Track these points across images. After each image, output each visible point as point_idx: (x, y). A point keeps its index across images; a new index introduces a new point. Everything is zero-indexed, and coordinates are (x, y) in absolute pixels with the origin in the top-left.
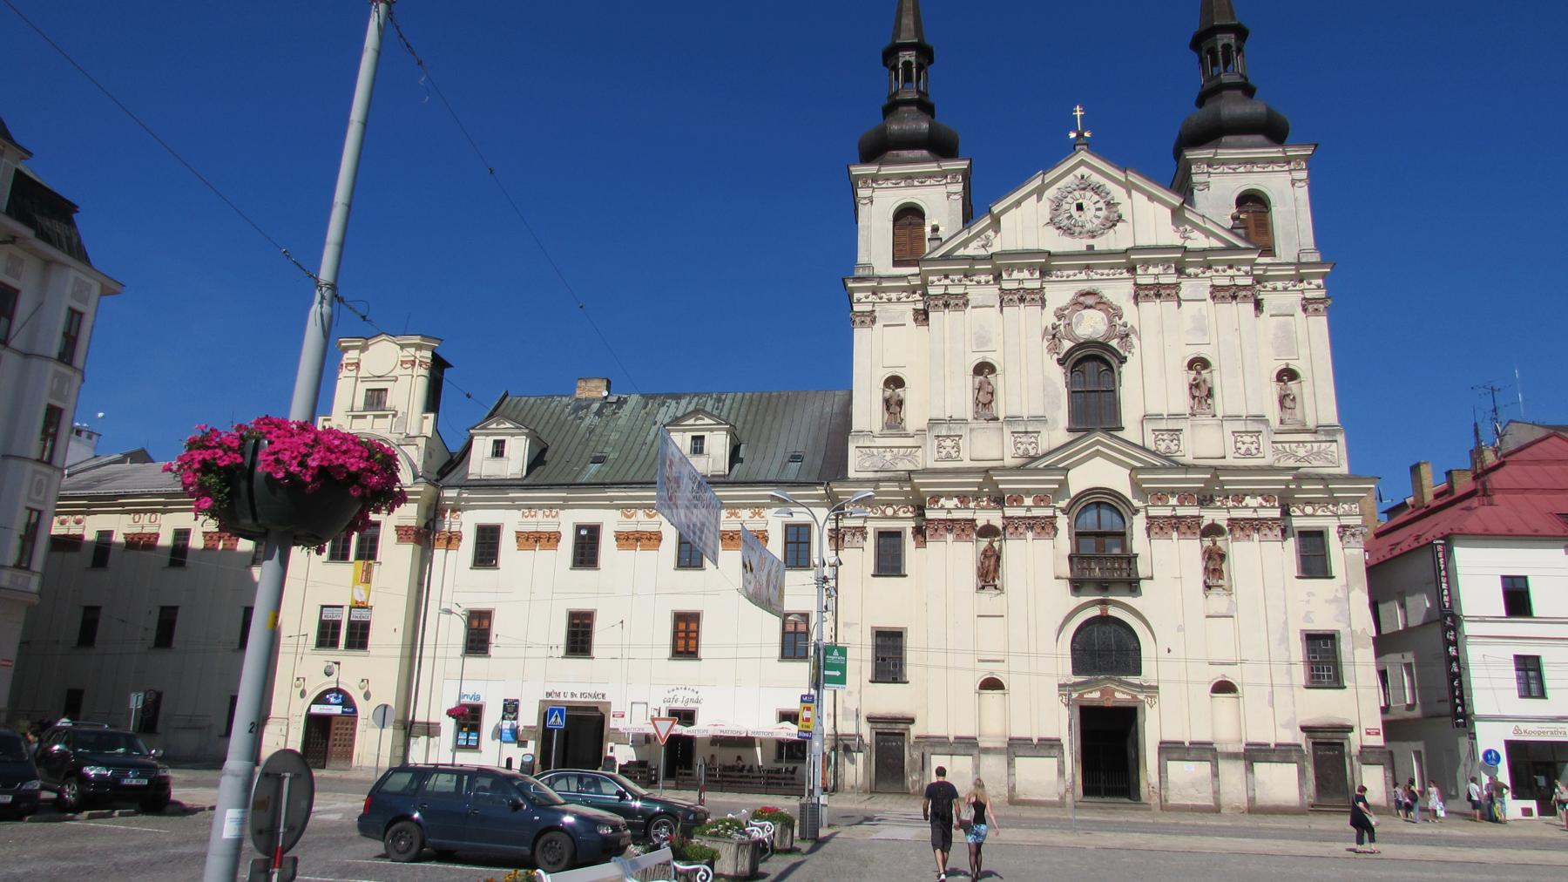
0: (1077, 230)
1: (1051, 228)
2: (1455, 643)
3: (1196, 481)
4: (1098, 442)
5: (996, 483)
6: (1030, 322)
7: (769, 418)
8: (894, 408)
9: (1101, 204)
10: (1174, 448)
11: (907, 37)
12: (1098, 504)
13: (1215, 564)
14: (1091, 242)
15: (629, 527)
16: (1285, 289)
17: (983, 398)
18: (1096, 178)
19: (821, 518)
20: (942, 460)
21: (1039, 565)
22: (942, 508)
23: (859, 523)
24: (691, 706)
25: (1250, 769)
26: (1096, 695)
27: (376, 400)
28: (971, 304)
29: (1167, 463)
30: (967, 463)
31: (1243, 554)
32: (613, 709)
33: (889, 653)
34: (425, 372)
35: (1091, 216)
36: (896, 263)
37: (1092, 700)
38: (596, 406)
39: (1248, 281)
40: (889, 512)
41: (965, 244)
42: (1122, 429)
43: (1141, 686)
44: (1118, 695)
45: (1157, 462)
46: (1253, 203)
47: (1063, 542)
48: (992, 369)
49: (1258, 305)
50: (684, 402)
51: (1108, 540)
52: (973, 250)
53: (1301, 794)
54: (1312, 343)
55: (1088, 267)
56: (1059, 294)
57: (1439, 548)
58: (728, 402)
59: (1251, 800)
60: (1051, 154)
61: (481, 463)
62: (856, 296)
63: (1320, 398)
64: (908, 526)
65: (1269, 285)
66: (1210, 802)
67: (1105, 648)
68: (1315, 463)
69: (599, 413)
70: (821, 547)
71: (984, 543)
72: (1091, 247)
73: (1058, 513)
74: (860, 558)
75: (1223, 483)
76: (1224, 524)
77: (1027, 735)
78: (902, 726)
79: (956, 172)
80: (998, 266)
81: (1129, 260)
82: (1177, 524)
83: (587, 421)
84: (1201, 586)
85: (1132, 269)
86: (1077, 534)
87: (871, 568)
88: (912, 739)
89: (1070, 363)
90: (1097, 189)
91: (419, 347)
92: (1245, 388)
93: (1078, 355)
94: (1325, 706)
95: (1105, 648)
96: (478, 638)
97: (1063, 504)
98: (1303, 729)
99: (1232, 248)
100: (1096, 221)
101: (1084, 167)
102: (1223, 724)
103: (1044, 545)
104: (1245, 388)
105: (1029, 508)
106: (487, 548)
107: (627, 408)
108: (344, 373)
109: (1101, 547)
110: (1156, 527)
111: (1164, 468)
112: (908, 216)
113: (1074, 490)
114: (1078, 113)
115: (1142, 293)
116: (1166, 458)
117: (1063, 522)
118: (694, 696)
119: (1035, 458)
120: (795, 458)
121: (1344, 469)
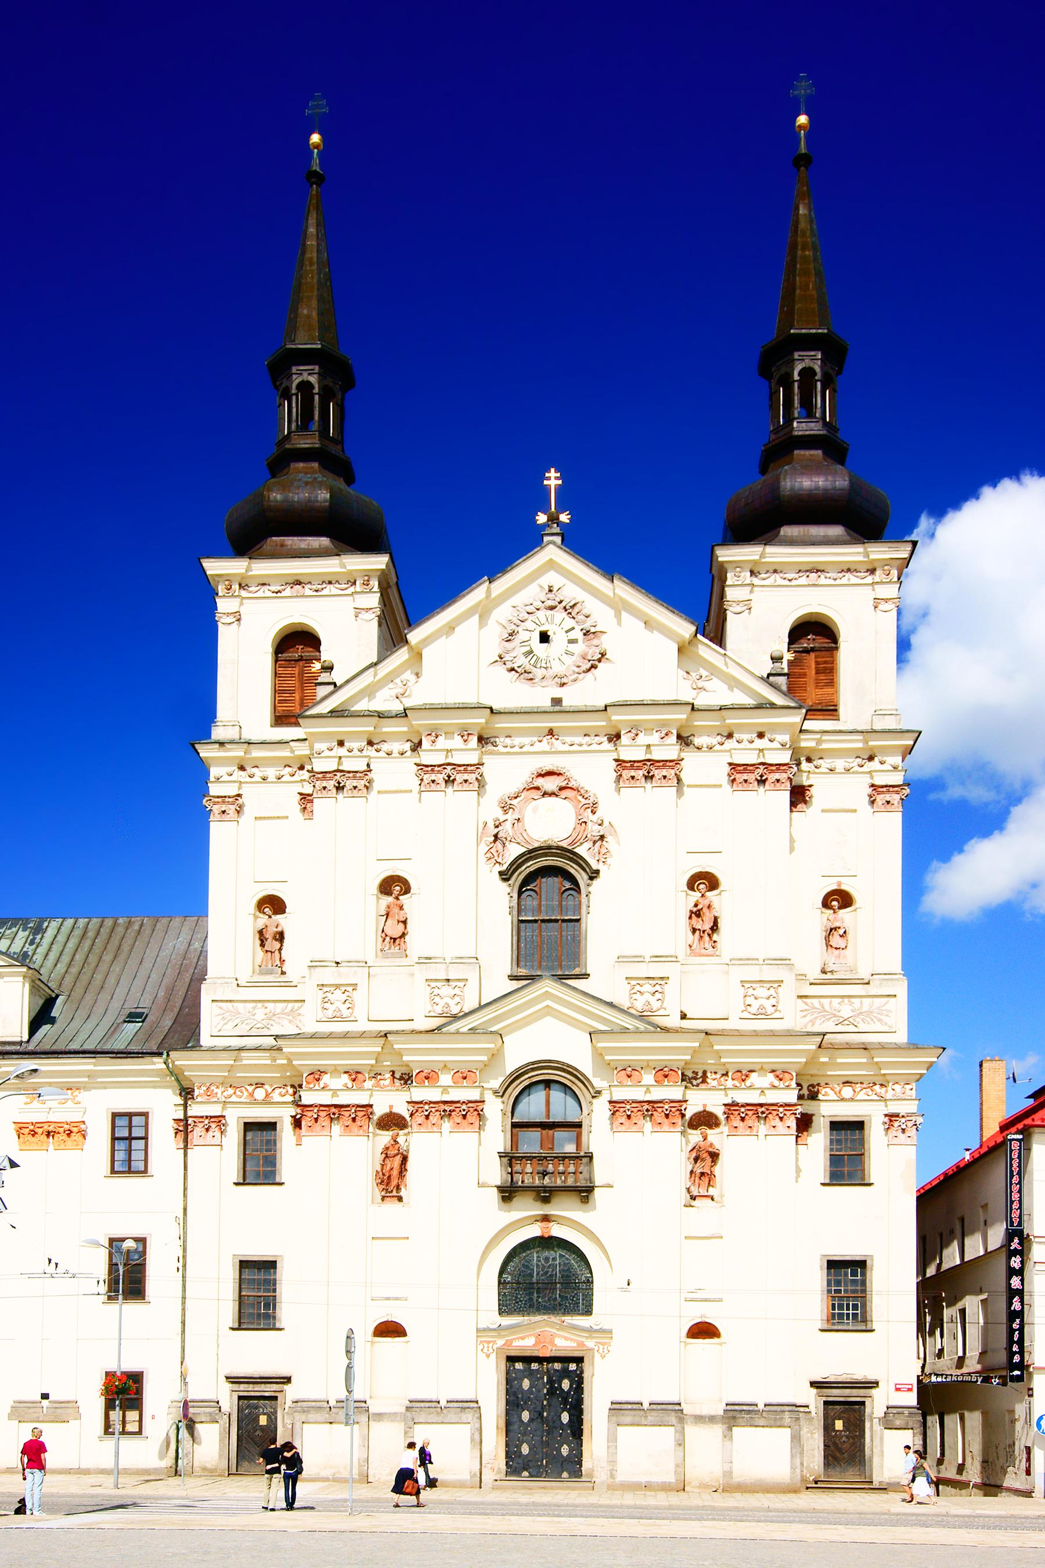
0: (539, 673)
1: (501, 670)
2: (1020, 1272)
3: (677, 1051)
4: (547, 995)
5: (400, 1054)
6: (462, 813)
7: (108, 958)
8: (272, 945)
9: (577, 634)
10: (656, 1005)
11: (305, 341)
12: (548, 1084)
14: (558, 693)
15: (36, 1113)
17: (395, 930)
18: (571, 593)
19: (162, 1106)
20: (333, 1019)
21: (460, 1167)
23: (215, 1110)
25: (728, 1435)
28: (376, 786)
29: (642, 1026)
37: (523, 1348)
39: (785, 757)
40: (260, 1094)
41: (369, 692)
42: (585, 976)
43: (590, 1330)
45: (630, 1023)
46: (814, 635)
47: (496, 1135)
48: (406, 889)
49: (799, 795)
51: (559, 1134)
52: (384, 701)
53: (793, 1468)
56: (507, 771)
57: (1015, 1145)
59: (728, 1474)
60: (501, 548)
64: (284, 1115)
65: (825, 764)
66: (671, 1478)
67: (545, 1279)
68: (862, 1027)
71: (385, 1137)
72: (557, 701)
73: (489, 1097)
74: (221, 1156)
75: (719, 1054)
76: (719, 1112)
77: (322, 1396)
78: (275, 1387)
79: (367, 575)
80: (415, 726)
86: (514, 1125)
87: (235, 1175)
88: (289, 1403)
90: (570, 610)
92: (770, 918)
93: (532, 866)
94: (846, 1356)
95: (545, 1279)
97: (496, 1083)
98: (813, 1384)
102: (707, 1379)
103: (466, 1139)
104: (770, 918)
105: (445, 1089)
111: (637, 1031)
112: (297, 644)
113: (513, 1061)
114: (553, 479)
115: (627, 774)
116: (641, 1017)
117: (495, 1109)
119: (455, 1018)
120: (133, 1017)
121: (901, 1037)
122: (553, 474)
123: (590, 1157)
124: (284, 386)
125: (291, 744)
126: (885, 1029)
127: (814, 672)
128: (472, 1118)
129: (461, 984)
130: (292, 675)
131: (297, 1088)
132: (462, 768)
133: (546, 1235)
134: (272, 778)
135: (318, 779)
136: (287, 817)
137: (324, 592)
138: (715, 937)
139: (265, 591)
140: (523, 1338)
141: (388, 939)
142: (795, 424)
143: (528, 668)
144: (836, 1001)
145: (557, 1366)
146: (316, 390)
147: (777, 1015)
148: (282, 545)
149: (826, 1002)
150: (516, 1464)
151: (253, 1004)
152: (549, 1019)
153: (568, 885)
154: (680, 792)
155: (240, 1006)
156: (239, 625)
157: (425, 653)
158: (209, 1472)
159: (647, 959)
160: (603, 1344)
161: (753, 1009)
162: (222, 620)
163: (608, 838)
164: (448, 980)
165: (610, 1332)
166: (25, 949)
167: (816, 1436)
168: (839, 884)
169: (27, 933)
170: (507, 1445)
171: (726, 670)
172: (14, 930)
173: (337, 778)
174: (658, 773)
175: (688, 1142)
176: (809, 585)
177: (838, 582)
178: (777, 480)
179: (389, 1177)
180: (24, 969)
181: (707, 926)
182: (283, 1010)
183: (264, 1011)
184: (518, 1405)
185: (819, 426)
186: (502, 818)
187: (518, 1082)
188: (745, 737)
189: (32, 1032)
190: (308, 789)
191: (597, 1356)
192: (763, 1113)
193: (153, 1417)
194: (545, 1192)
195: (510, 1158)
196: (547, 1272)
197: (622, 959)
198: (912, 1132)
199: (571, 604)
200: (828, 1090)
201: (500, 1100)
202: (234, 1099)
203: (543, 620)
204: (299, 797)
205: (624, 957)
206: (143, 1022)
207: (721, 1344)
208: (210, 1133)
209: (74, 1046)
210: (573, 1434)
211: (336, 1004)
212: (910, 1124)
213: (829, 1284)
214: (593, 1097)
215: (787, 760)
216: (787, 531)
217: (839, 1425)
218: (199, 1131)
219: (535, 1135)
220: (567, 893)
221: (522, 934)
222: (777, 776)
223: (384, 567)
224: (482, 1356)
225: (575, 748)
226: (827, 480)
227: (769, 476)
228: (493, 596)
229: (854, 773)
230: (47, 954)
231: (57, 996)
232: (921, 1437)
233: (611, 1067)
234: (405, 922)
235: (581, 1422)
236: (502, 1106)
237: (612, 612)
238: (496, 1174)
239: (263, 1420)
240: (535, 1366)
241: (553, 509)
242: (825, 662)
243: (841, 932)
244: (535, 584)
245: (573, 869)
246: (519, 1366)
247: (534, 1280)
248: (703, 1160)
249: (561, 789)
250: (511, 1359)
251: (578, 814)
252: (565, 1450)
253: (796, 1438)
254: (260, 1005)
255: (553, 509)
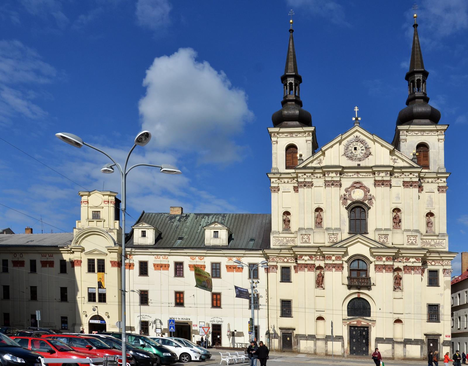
0: (354, 158)
6: (336, 193)
7: (242, 224)
9: (363, 148)
10: (386, 241)
12: (358, 260)
13: (398, 281)
14: (359, 163)
16: (432, 182)
18: (362, 137)
21: (337, 280)
22: (303, 260)
23: (275, 264)
24: (219, 323)
26: (355, 323)
27: (96, 216)
29: (382, 246)
30: (312, 244)
31: (407, 279)
32: (193, 323)
33: (286, 308)
34: (113, 205)
35: (359, 153)
36: (287, 168)
38: (178, 218)
39: (417, 180)
40: (286, 260)
41: (312, 162)
42: (368, 233)
43: (370, 320)
44: (363, 323)
45: (379, 246)
46: (423, 147)
47: (346, 272)
50: (211, 217)
52: (314, 164)
54: (439, 202)
55: (358, 172)
56: (347, 183)
58: (227, 217)
59: (405, 356)
60: (344, 127)
61: (137, 239)
62: (272, 180)
63: (441, 224)
64: (292, 265)
67: (359, 308)
68: (437, 247)
69: (179, 220)
70: (262, 271)
71: (318, 272)
72: (359, 165)
73: (344, 263)
74: (276, 276)
76: (402, 268)
79: (309, 131)
80: (325, 170)
81: (373, 170)
82: (385, 267)
83: (175, 224)
84: (392, 288)
85: (374, 174)
86: (350, 270)
87: (279, 278)
88: (295, 335)
89: (350, 208)
91: (110, 196)
92: (414, 220)
94: (433, 328)
95: (359, 308)
96: (144, 298)
98: (425, 335)
99: (413, 167)
100: (361, 155)
101: (358, 132)
102: (399, 333)
104: (414, 220)
106: (144, 269)
107: (190, 219)
108: (83, 205)
109: (358, 274)
110: (378, 268)
111: (381, 248)
112: (291, 149)
114: (356, 109)
116: (382, 244)
117: (345, 265)
118: (221, 320)
119: (336, 243)
120: (252, 240)
122: (356, 108)
123: (370, 278)
124: (285, 83)
125: (292, 174)
126: (443, 247)
127: (422, 157)
128: (340, 268)
129: (337, 235)
130: (290, 156)
131: (296, 259)
132: (336, 181)
133: (359, 297)
134: (286, 182)
135: (299, 183)
136: (290, 192)
137: (298, 136)
138: (400, 224)
139: (413, 133)
140: (353, 322)
141: (317, 223)
142: (416, 93)
143: (351, 156)
144: (430, 240)
145: (362, 329)
146: (293, 85)
147: (416, 244)
148: (287, 124)
149: (427, 240)
150: (352, 352)
151: (283, 238)
152: (359, 243)
153: (362, 210)
154: (391, 187)
155: (280, 238)
156: (277, 144)
157: (326, 152)
158: (277, 351)
159: (383, 230)
160: (374, 324)
161: (410, 243)
162: (273, 143)
163: (373, 199)
164: (333, 234)
165: (375, 321)
166: (222, 222)
167: (426, 347)
168: (430, 211)
169: (221, 217)
170: (350, 347)
171: (402, 158)
172: (218, 216)
173: (304, 183)
174: (385, 183)
175: (394, 274)
176: (421, 135)
177: (429, 134)
178: (412, 108)
179: (319, 282)
180: (227, 228)
181: (398, 222)
182: (291, 239)
183: (286, 240)
184: (352, 338)
185: (422, 93)
186: (346, 194)
187: (351, 259)
188: (407, 174)
189: (229, 243)
190: (296, 185)
191: (372, 327)
192: (413, 268)
193: (262, 337)
194: (359, 286)
195: (349, 278)
196: (359, 306)
197: (377, 230)
198: (450, 274)
199: (362, 140)
200: (428, 263)
201: (347, 263)
202: (279, 261)
203: (355, 145)
204: (293, 187)
205: (377, 229)
206: (254, 241)
207: (403, 324)
208: (274, 269)
209: (239, 247)
210: (366, 345)
211: (305, 239)
212: (449, 271)
213: (429, 310)
214: (370, 264)
215: (418, 180)
216: (415, 121)
217: (431, 345)
218: (271, 269)
219: (356, 272)
220: (362, 213)
221: (351, 222)
222: (415, 184)
223: (313, 130)
224: (344, 326)
225: (364, 177)
226: (425, 109)
227: (410, 106)
228: (343, 138)
229: (434, 183)
230: (227, 223)
231: (232, 234)
232: (452, 348)
233: (374, 256)
234: (322, 219)
235: (368, 342)
236: (347, 265)
237: (373, 142)
238: (346, 282)
239: (288, 339)
240: (356, 328)
241: (357, 116)
242: (426, 154)
243: (431, 223)
244: (352, 135)
245: (364, 207)
246: (352, 328)
247: (356, 308)
248: (398, 279)
249: (360, 187)
250: (351, 327)
251: (365, 193)
252: (364, 349)
253: (422, 348)
254: (285, 238)
255: (357, 116)
